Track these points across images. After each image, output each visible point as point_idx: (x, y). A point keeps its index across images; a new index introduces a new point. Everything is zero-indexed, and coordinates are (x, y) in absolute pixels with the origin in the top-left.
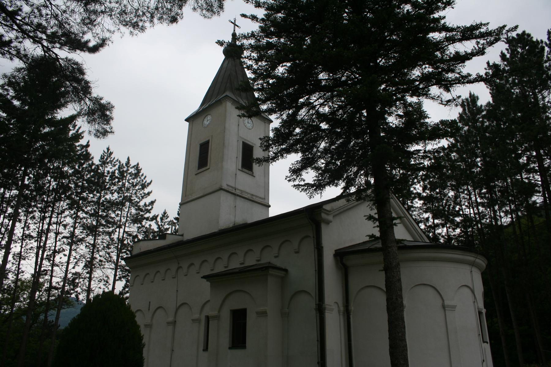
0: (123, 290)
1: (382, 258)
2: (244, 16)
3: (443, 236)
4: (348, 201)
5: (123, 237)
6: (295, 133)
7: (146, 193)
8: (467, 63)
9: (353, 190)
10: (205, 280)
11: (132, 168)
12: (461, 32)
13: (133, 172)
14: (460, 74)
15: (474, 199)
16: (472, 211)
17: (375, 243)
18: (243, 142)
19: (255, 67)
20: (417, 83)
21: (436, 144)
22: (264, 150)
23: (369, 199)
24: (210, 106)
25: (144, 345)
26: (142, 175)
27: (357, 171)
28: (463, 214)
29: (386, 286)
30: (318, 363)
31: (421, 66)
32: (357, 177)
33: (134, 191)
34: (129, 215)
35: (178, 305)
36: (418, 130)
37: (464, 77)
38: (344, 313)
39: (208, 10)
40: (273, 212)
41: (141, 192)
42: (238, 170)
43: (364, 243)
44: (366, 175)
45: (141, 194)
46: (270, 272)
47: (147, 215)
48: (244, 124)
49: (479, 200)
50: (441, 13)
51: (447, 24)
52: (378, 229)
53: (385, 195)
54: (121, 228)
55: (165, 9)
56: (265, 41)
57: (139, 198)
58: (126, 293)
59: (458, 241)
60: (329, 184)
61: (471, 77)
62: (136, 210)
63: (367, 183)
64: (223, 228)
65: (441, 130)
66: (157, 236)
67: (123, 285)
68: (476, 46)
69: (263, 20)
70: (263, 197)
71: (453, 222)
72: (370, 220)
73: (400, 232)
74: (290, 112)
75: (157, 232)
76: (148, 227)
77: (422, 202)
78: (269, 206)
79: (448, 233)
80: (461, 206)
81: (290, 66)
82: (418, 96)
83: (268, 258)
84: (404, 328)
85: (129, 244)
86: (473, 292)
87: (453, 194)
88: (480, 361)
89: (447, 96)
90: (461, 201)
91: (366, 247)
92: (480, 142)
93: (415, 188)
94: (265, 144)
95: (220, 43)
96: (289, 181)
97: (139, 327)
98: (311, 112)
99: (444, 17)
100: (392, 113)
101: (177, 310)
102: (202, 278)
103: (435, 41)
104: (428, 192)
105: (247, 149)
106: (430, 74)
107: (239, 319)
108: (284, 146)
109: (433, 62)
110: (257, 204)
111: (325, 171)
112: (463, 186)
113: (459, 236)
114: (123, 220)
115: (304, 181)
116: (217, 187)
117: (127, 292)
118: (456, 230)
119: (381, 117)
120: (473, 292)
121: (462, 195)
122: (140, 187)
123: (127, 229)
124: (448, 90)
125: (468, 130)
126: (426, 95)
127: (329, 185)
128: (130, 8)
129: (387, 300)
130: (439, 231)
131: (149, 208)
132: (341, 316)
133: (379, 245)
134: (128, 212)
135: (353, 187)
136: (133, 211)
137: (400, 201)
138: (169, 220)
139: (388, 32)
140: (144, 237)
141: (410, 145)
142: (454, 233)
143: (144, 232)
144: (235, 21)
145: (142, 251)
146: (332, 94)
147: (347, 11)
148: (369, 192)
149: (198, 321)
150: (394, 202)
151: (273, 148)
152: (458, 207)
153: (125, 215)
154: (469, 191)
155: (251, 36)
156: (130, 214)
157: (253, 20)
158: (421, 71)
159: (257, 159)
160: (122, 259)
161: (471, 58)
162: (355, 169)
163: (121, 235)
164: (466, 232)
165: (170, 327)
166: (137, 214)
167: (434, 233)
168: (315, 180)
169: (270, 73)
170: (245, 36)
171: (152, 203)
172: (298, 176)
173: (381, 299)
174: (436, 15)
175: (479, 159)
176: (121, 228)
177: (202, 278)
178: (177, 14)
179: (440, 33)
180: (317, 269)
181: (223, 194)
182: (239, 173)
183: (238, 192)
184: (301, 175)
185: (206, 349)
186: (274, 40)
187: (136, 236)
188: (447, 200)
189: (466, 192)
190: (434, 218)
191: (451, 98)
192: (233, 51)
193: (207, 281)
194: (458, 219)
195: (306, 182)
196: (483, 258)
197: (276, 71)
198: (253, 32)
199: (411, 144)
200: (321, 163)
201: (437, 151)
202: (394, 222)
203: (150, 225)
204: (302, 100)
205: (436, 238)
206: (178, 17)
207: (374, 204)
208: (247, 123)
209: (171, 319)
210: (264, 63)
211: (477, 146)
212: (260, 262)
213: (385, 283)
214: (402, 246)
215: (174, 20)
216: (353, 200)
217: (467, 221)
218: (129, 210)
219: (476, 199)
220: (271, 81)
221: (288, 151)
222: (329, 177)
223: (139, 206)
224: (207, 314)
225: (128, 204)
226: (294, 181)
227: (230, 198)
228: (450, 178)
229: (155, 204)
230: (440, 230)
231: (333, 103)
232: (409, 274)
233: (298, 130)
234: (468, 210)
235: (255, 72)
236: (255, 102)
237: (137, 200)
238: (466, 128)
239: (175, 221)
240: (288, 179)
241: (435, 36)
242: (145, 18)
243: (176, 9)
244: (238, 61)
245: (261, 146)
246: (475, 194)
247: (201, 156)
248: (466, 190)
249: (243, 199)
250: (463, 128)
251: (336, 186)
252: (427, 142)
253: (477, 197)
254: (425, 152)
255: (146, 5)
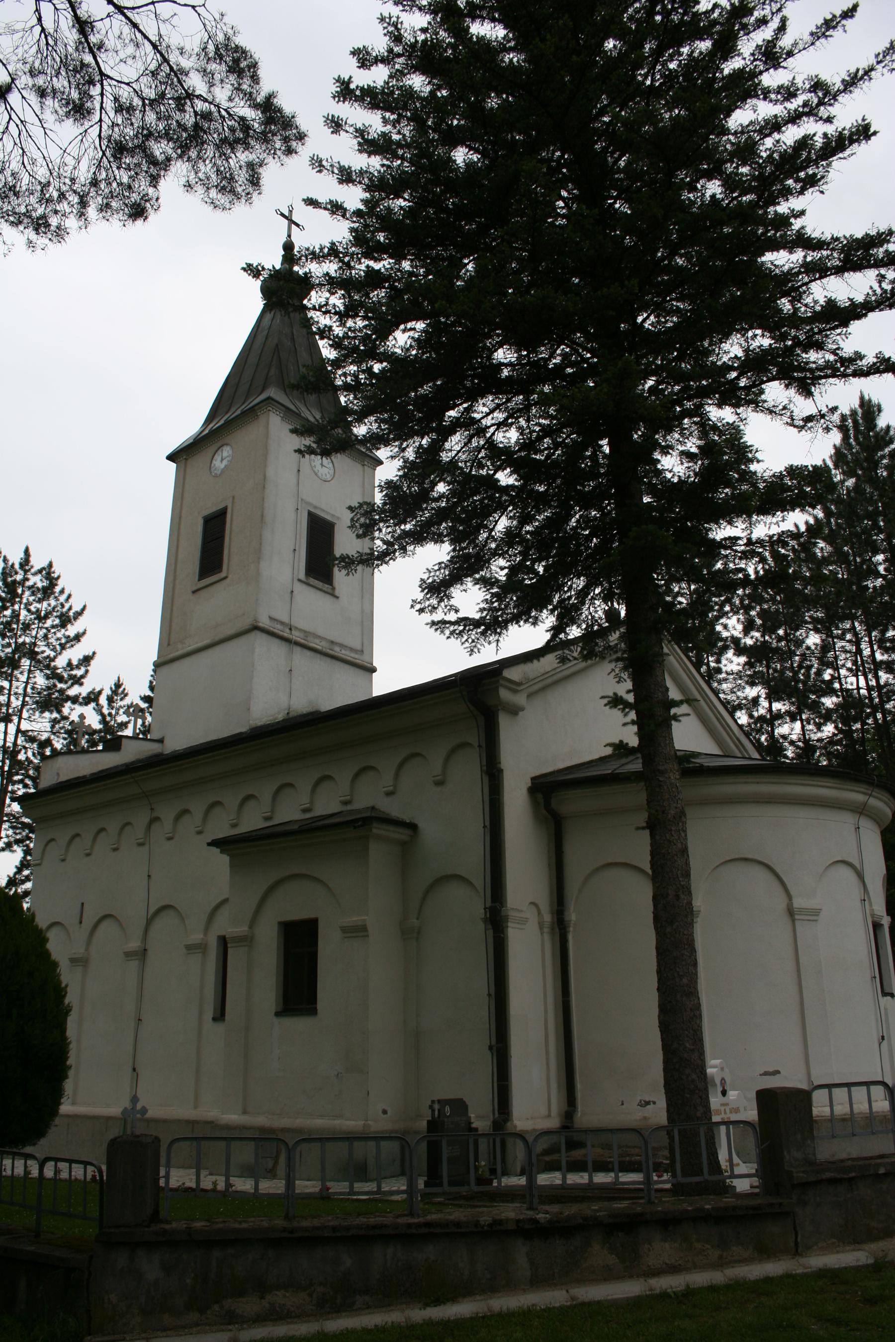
0: (16, 874)
1: (642, 797)
2: (311, 202)
3: (792, 743)
4: (563, 660)
5: (15, 744)
6: (435, 495)
7: (72, 635)
8: (855, 326)
9: (574, 632)
10: (216, 850)
11: (35, 574)
12: (842, 251)
13: (40, 585)
14: (836, 355)
15: (867, 652)
16: (862, 683)
17: (624, 761)
18: (311, 515)
19: (338, 331)
20: (734, 374)
21: (777, 523)
22: (358, 536)
23: (614, 657)
24: (228, 424)
25: (68, 1010)
26: (62, 592)
27: (584, 587)
28: (841, 690)
29: (653, 864)
30: (491, 1048)
31: (743, 331)
32: (584, 604)
33: (42, 633)
34: (29, 690)
35: (152, 910)
36: (734, 488)
37: (846, 361)
38: (552, 929)
39: (222, 190)
40: (383, 684)
41: (59, 635)
42: (296, 581)
43: (602, 760)
44: (607, 597)
45: (58, 639)
46: (374, 831)
47: (73, 691)
48: (312, 468)
49: (879, 656)
50: (795, 203)
51: (808, 231)
52: (635, 728)
53: (651, 645)
54: (11, 721)
55: (115, 185)
56: (363, 267)
57: (54, 650)
58: (23, 882)
59: (829, 755)
60: (516, 619)
61: (864, 362)
62: (48, 677)
63: (611, 615)
64: (259, 723)
65: (789, 489)
66: (100, 741)
67: (18, 863)
68: (876, 286)
69: (358, 213)
70: (359, 647)
71: (815, 707)
72: (615, 706)
73: (688, 735)
74: (424, 442)
75: (100, 731)
76: (77, 719)
77: (743, 659)
78: (374, 670)
79: (804, 734)
80: (836, 669)
81: (423, 331)
82: (736, 406)
83: (369, 795)
84: (695, 964)
85: (31, 762)
86: (860, 876)
87: (818, 641)
88: (875, 1038)
89: (803, 407)
90: (836, 658)
91: (607, 769)
92: (885, 516)
93: (725, 627)
94: (362, 520)
95: (253, 271)
96: (421, 611)
97: (55, 965)
98: (474, 443)
99: (802, 213)
100: (672, 447)
101: (149, 922)
102: (209, 844)
103: (777, 271)
104: (757, 634)
105: (320, 531)
106: (769, 351)
107: (300, 943)
108: (408, 527)
109: (773, 323)
110: (347, 667)
111: (506, 588)
112: (842, 622)
113: (831, 741)
114: (16, 703)
115: (457, 611)
116: (246, 623)
117: (28, 878)
118: (824, 728)
119: (645, 454)
120: (860, 876)
121: (839, 644)
122: (57, 621)
123: (25, 726)
124: (808, 394)
125: (857, 486)
126: (756, 403)
127: (517, 623)
128: (26, 179)
129: (655, 898)
130: (783, 729)
131: (79, 673)
132: (547, 937)
133: (636, 765)
134: (27, 683)
135: (574, 627)
136: (40, 680)
137: (689, 658)
138: (127, 701)
139: (664, 248)
140: (68, 745)
141: (714, 526)
142: (819, 735)
143: (68, 732)
144: (291, 212)
145: (64, 778)
146: (526, 399)
147: (564, 194)
148: (614, 637)
149: (201, 948)
150: (675, 658)
151: (380, 530)
152: (830, 671)
153: (21, 691)
154: (856, 634)
155: (329, 255)
156: (33, 688)
157: (333, 213)
158: (744, 344)
159: (343, 558)
160: (13, 800)
161: (865, 315)
162: (581, 583)
163: (11, 739)
164: (848, 734)
165: (134, 965)
166: (48, 688)
167: (771, 735)
168: (484, 609)
169: (375, 347)
170: (313, 253)
171: (87, 660)
172: (441, 600)
173: (640, 895)
174: (783, 208)
175: (880, 557)
176: (11, 721)
177: (209, 844)
178: (146, 198)
179: (791, 253)
180: (487, 823)
181: (259, 641)
182: (299, 588)
183: (296, 636)
184: (449, 597)
185: (220, 1016)
186: (383, 265)
187: (48, 742)
188: (804, 656)
189: (848, 636)
190: (770, 698)
191: (814, 411)
192: (284, 289)
193: (222, 852)
194: (829, 702)
195: (461, 615)
196: (886, 796)
197: (390, 343)
198: (333, 244)
199: (717, 523)
200: (499, 568)
201: (780, 540)
202: (673, 711)
203: (82, 717)
204: (452, 413)
205: (775, 747)
206: (148, 205)
207: (625, 669)
208: (319, 467)
209: (134, 944)
210: (360, 323)
211: (875, 525)
212: (349, 807)
213: (650, 858)
214: (691, 767)
215: (138, 212)
216: (575, 659)
217: (852, 707)
218: (29, 678)
219: (873, 652)
220: (377, 367)
221: (419, 537)
222: (518, 600)
223: (56, 668)
224: (222, 933)
225: (28, 662)
226: (431, 612)
227: (278, 649)
228: (813, 602)
229: (93, 662)
230: (786, 726)
231: (528, 421)
232: (710, 836)
233: (441, 488)
234: (854, 679)
235: (337, 344)
236: (342, 418)
237: (49, 652)
238: (851, 482)
239: (144, 705)
240: (418, 607)
241: (781, 260)
242: (64, 206)
243: (143, 185)
244: (296, 316)
245: (352, 527)
246: (870, 642)
247: (207, 546)
248: (849, 630)
249: (308, 653)
250: (842, 482)
251: (534, 624)
252: (755, 517)
253: (875, 647)
254: (749, 542)
255: (68, 174)
